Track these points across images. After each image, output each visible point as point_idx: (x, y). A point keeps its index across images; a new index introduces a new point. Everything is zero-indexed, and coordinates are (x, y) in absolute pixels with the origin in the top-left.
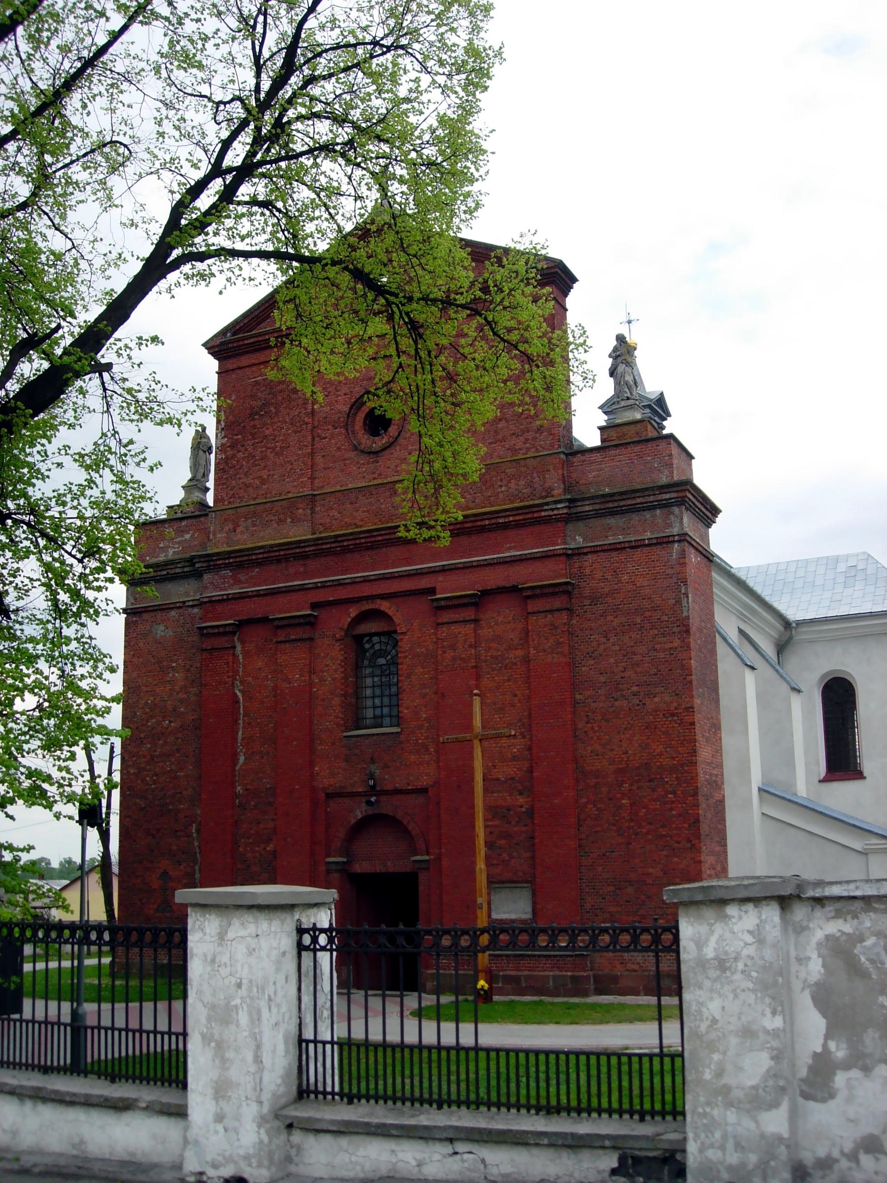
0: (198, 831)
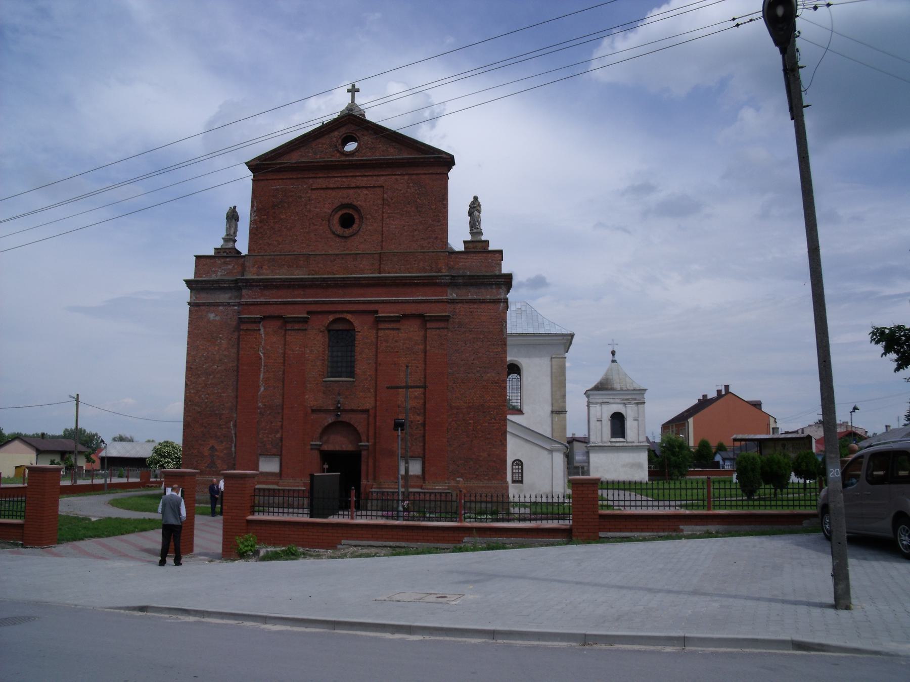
0: (235, 426)
